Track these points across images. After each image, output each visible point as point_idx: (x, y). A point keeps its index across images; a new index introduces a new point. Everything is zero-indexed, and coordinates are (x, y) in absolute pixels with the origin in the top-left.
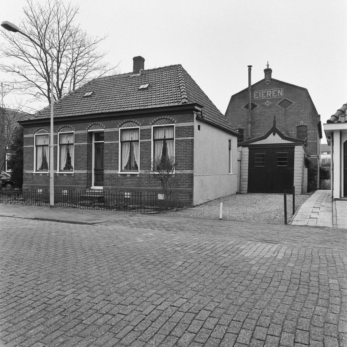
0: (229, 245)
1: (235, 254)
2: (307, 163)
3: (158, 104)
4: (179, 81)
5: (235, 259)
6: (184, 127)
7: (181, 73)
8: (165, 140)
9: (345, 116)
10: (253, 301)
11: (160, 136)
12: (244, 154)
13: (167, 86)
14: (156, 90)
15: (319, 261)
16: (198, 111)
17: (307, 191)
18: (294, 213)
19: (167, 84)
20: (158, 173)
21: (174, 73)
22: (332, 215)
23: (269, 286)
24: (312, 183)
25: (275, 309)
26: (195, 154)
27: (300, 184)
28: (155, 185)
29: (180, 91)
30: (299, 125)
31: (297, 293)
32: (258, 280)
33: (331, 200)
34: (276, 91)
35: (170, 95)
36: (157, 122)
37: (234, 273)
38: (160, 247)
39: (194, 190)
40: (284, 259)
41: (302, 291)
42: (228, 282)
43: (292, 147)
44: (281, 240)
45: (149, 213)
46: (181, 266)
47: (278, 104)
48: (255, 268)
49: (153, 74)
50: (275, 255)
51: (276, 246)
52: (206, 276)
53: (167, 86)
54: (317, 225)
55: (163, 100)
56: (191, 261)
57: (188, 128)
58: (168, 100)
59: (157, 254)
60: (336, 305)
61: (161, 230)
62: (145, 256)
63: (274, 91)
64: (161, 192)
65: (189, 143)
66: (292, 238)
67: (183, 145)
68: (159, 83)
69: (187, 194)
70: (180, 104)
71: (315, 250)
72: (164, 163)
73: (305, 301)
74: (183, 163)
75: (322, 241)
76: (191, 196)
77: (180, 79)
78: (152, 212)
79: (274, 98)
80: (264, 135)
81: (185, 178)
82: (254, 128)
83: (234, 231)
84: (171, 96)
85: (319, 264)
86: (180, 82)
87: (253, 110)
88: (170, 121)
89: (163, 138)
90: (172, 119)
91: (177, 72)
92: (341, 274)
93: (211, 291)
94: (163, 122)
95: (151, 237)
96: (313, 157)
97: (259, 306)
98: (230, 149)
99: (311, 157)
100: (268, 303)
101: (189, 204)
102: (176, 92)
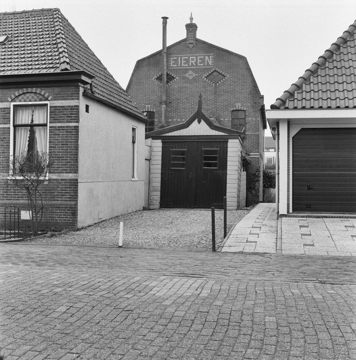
0: (134, 283)
1: (142, 294)
2: (245, 164)
3: (22, 69)
4: (56, 35)
5: (143, 299)
6: (64, 107)
7: (58, 23)
8: (32, 126)
9: (294, 100)
10: (168, 349)
11: (25, 120)
12: (155, 149)
13: (36, 42)
14: (18, 47)
15: (255, 296)
16: (85, 83)
17: (245, 204)
18: (225, 236)
19: (36, 38)
20: (21, 178)
21: (47, 22)
22: (276, 238)
23: (189, 330)
24: (252, 193)
25: (197, 356)
26: (80, 149)
27: (235, 195)
28: (15, 197)
29: (57, 51)
30: (235, 109)
31: (224, 336)
32: (175, 324)
33: (276, 217)
34: (203, 57)
35: (42, 57)
36: (20, 98)
37: (142, 318)
38: (31, 289)
39: (79, 204)
40: (210, 296)
41: (231, 333)
42: (134, 329)
43: (224, 140)
44: (207, 272)
45: (7, 240)
46: (64, 312)
47: (206, 77)
48: (171, 310)
49: (13, 20)
50: (198, 292)
51: (200, 281)
52: (104, 324)
53: (36, 42)
54: (256, 251)
55: (30, 63)
56: (79, 305)
57: (71, 109)
58: (38, 64)
59: (27, 299)
60: (271, 345)
61: (29, 265)
62: (9, 302)
63: (200, 57)
64: (26, 207)
65: (72, 132)
66: (222, 270)
67: (62, 135)
68: (23, 36)
69: (68, 210)
70: (58, 71)
71: (252, 283)
72: (31, 163)
73: (234, 344)
74: (62, 162)
75: (261, 272)
76: (74, 213)
77: (57, 32)
78: (13, 239)
79: (200, 67)
80: (184, 121)
81: (64, 185)
82: (170, 112)
83: (140, 263)
84: (43, 58)
85: (255, 300)
86: (58, 36)
87: (169, 84)
88: (41, 97)
89: (29, 123)
90: (45, 93)
91: (52, 20)
92: (281, 310)
93: (110, 342)
94: (30, 98)
95: (15, 275)
96: (253, 155)
97: (176, 354)
98: (134, 142)
99: (251, 155)
100: (188, 350)
101: (71, 225)
102: (51, 52)
